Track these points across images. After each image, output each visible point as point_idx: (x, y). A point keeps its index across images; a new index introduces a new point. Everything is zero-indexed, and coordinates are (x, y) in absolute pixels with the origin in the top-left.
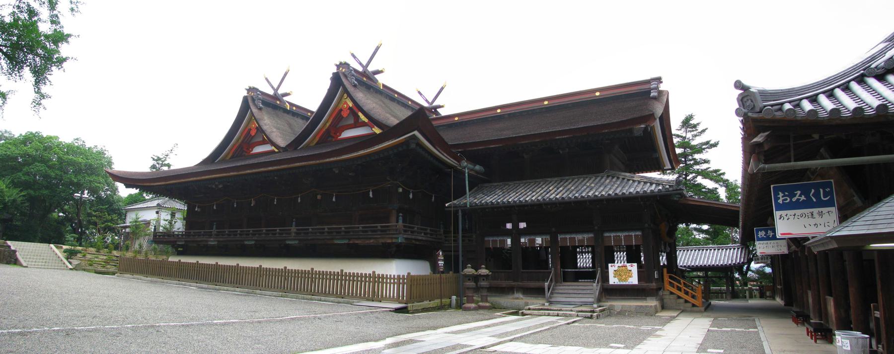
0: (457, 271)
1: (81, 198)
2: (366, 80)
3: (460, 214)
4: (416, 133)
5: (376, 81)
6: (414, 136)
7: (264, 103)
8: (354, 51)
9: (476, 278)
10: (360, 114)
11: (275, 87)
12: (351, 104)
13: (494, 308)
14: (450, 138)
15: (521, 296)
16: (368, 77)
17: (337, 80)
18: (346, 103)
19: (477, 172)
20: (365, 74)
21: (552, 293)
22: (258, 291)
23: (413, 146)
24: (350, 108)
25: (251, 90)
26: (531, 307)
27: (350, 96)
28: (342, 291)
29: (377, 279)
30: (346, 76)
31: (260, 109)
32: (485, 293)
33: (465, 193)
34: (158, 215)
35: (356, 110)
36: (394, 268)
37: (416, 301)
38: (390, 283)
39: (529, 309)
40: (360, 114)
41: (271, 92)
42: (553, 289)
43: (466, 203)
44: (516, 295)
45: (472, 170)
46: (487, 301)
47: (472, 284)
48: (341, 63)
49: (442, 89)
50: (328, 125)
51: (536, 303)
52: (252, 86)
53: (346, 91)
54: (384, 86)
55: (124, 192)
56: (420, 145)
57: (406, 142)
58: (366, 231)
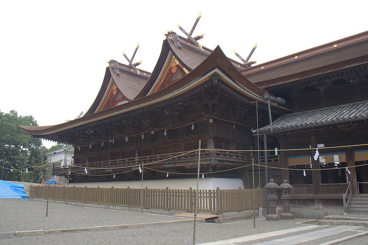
0: (263, 186)
1: (9, 148)
2: (191, 44)
3: (265, 138)
4: (216, 70)
5: (197, 45)
6: (216, 74)
7: (121, 70)
8: (180, 23)
9: (279, 192)
10: (184, 69)
11: (130, 59)
12: (178, 63)
13: (296, 216)
14: (253, 80)
15: (321, 207)
16: (192, 43)
17: (166, 46)
18: (174, 62)
19: (279, 104)
20: (189, 40)
21: (349, 204)
22: (111, 207)
23: (215, 82)
24: (178, 66)
25: (111, 62)
26: (329, 216)
27: (177, 57)
28: (168, 203)
29: (192, 194)
30: (173, 42)
31: (118, 75)
32: (286, 204)
33: (269, 123)
34: (64, 157)
35: (181, 65)
36: (210, 185)
37: (221, 211)
38: (204, 197)
39: (328, 219)
40: (184, 69)
41: (127, 63)
42: (351, 200)
43: (270, 129)
44: (316, 206)
45: (274, 101)
46: (289, 212)
47: (275, 196)
48: (169, 33)
49: (254, 50)
50: (163, 80)
51: (334, 212)
52: (112, 59)
53: (174, 54)
54: (203, 48)
55: (48, 144)
56: (221, 80)
57: (210, 80)
58: (187, 156)
